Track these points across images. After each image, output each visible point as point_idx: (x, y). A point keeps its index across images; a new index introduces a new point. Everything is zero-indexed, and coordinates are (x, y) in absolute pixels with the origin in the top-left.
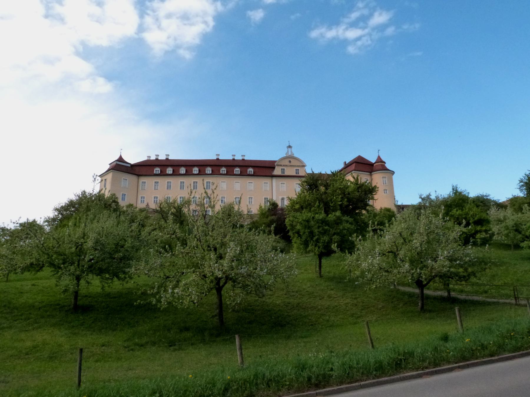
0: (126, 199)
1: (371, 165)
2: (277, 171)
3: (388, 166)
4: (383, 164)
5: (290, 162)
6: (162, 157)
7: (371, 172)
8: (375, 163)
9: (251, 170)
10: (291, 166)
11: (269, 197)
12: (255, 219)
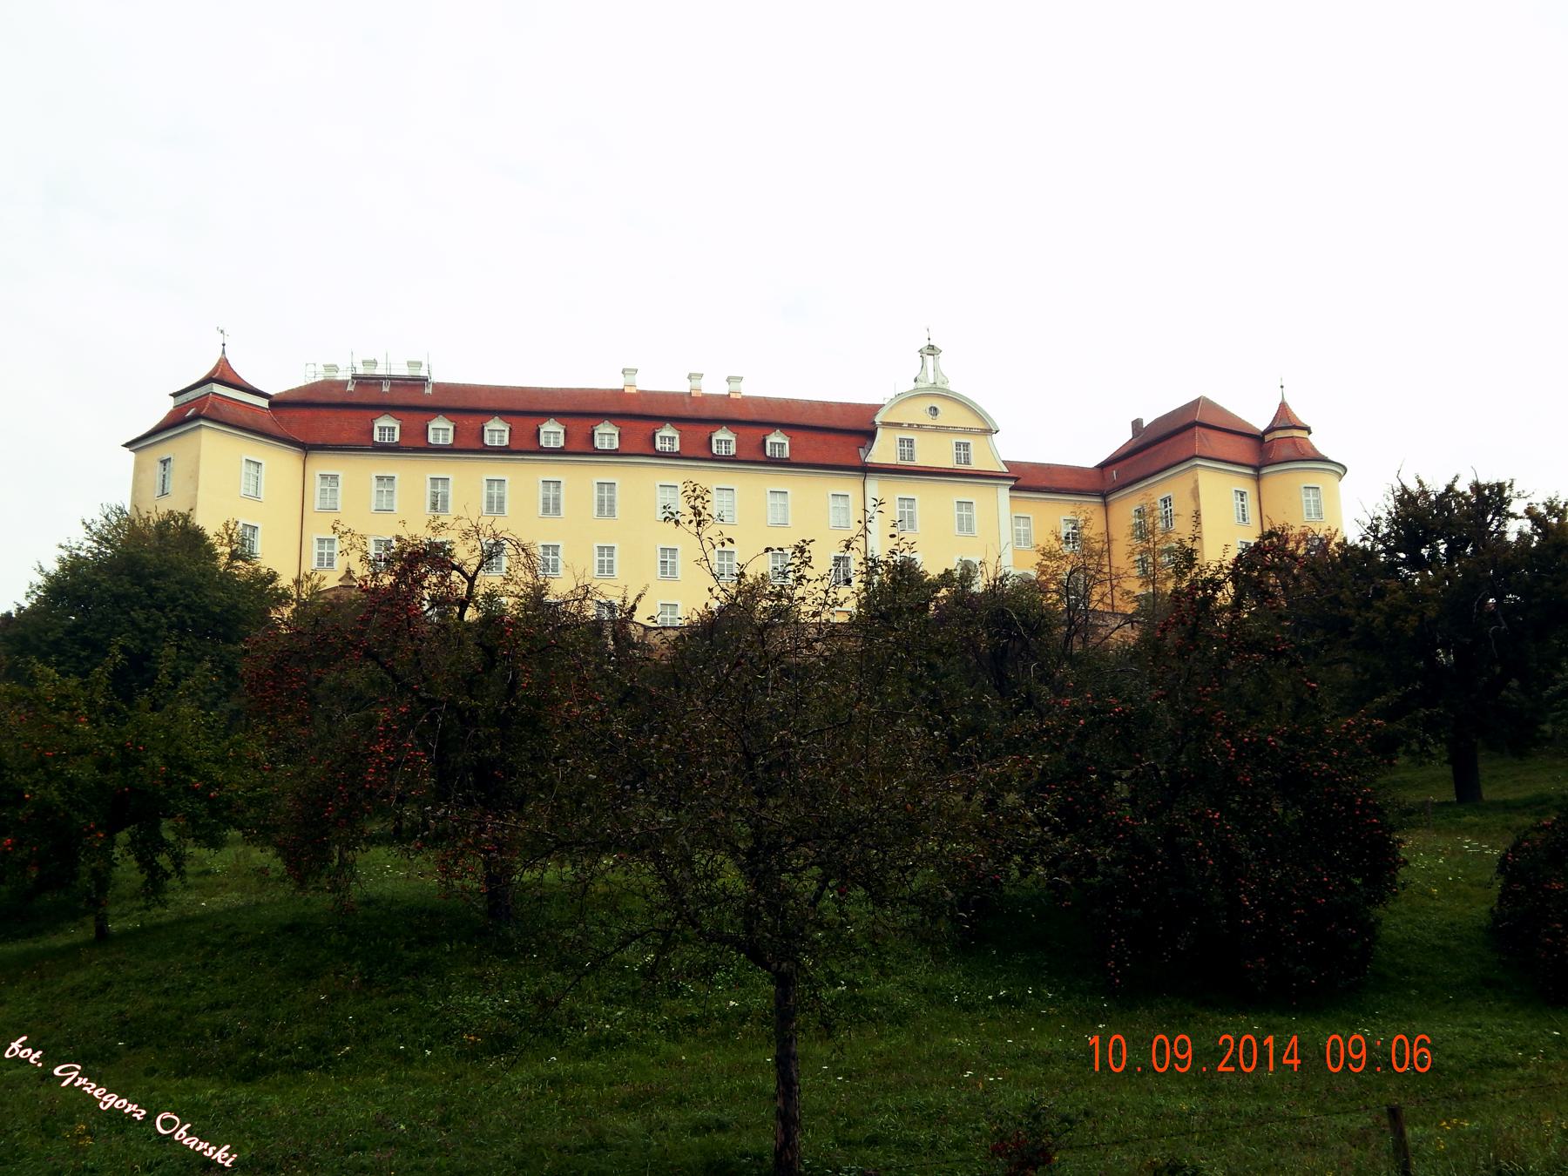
2: (883, 450)
3: (1320, 441)
4: (1296, 433)
5: (934, 411)
9: (777, 441)
10: (938, 429)
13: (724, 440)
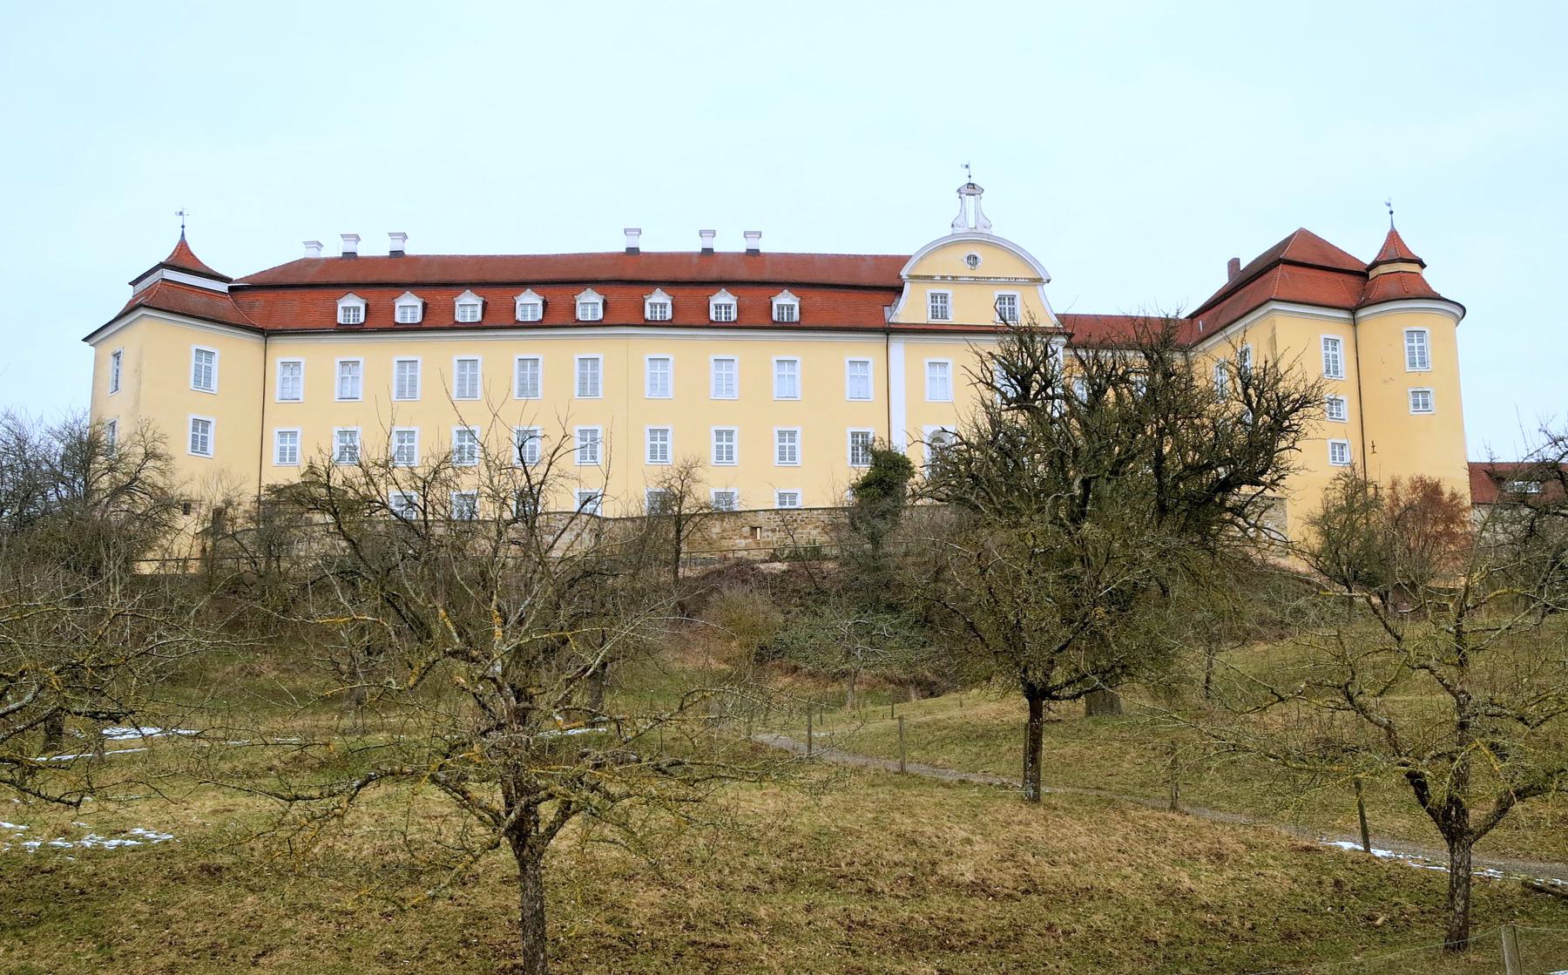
0: (210, 447)
1: (1362, 274)
2: (911, 308)
3: (1433, 278)
4: (1415, 268)
5: (973, 259)
6: (374, 246)
7: (1353, 311)
8: (1375, 264)
11: (876, 431)
12: (810, 534)
13: (529, 304)
